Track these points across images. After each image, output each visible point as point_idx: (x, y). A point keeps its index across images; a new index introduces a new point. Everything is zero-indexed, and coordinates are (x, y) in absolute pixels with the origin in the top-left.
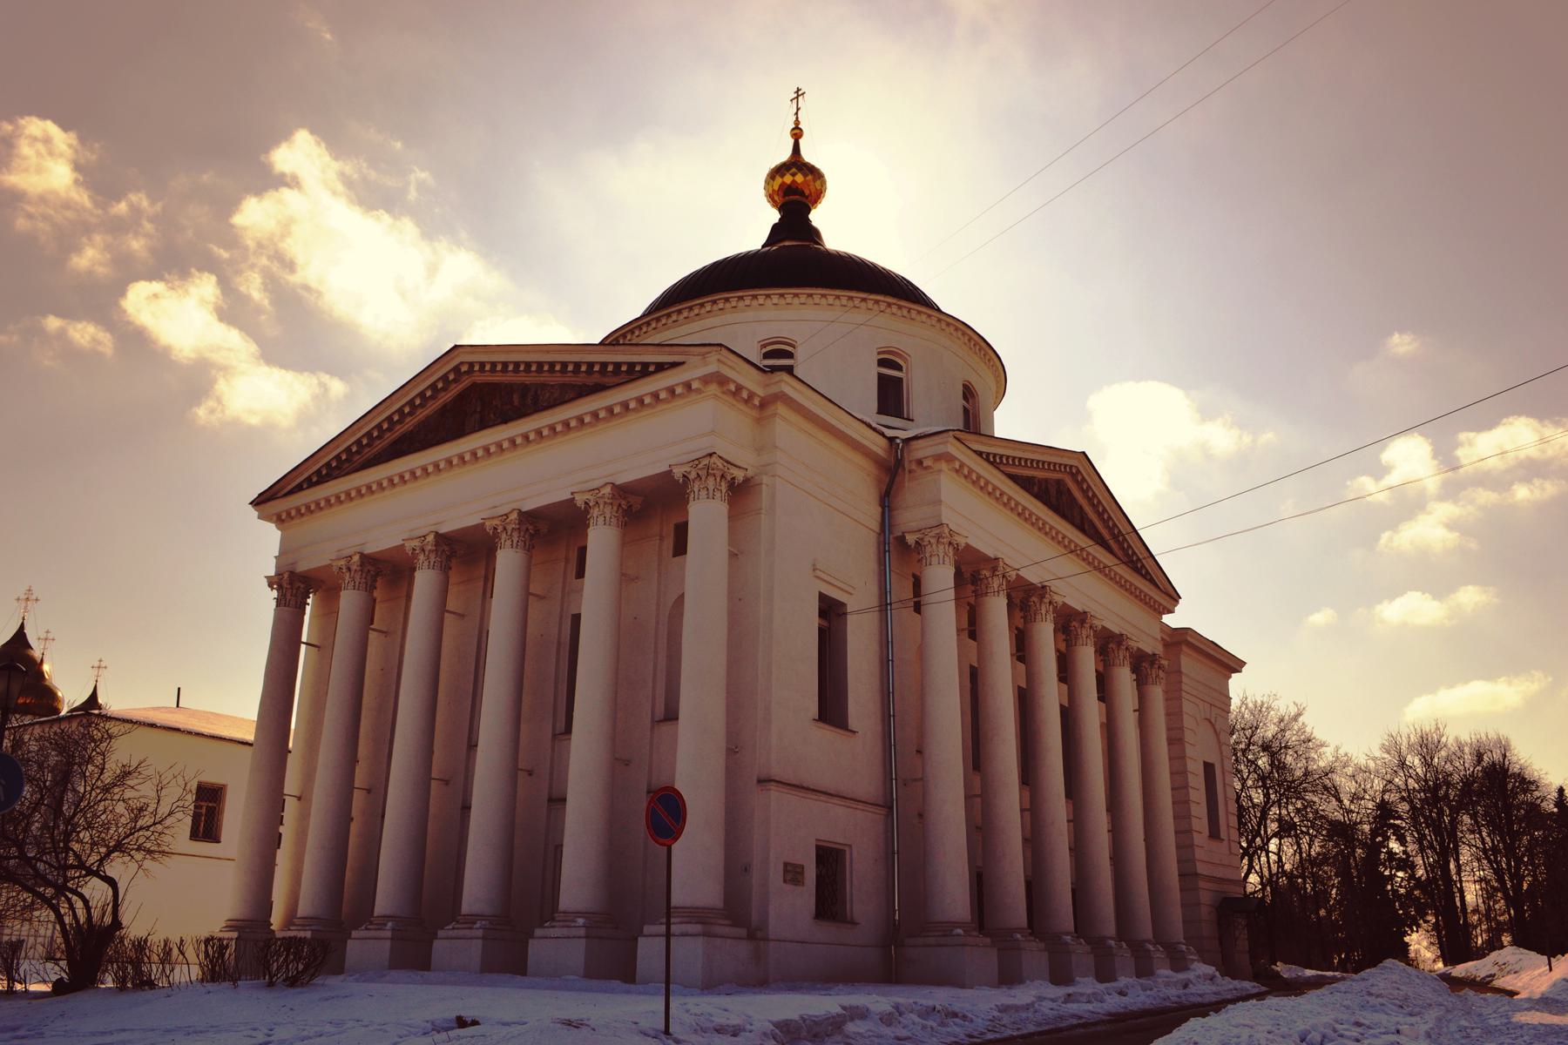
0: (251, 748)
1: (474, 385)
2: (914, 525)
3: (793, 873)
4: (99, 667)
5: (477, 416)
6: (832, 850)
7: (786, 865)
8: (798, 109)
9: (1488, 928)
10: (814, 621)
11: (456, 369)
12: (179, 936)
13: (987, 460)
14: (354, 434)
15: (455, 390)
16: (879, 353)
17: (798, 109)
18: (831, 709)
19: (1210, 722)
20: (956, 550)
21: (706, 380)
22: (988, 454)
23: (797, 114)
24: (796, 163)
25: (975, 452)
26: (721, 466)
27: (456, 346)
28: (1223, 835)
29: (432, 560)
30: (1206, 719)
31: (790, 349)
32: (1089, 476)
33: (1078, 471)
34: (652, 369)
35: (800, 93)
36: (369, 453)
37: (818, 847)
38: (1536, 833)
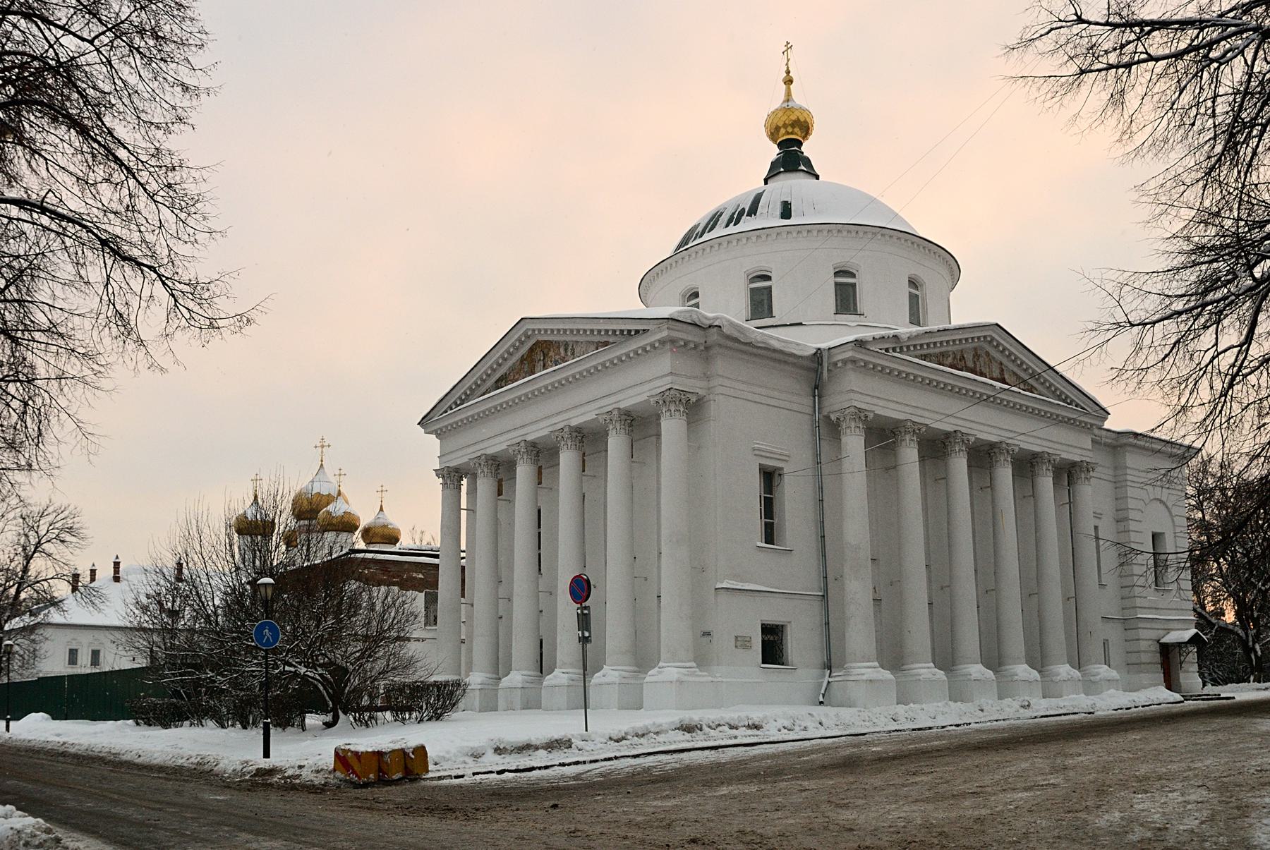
0: (4, 729)
1: (538, 342)
2: (836, 407)
3: (742, 642)
4: (340, 475)
5: (542, 363)
6: (777, 626)
8: (788, 60)
10: (755, 484)
11: (525, 334)
12: (465, 773)
16: (837, 274)
17: (788, 60)
19: (1161, 501)
20: (865, 421)
21: (662, 342)
23: (787, 64)
24: (788, 106)
27: (522, 319)
29: (525, 457)
30: (1155, 499)
34: (633, 333)
35: (789, 46)
37: (762, 625)
38: (267, 631)
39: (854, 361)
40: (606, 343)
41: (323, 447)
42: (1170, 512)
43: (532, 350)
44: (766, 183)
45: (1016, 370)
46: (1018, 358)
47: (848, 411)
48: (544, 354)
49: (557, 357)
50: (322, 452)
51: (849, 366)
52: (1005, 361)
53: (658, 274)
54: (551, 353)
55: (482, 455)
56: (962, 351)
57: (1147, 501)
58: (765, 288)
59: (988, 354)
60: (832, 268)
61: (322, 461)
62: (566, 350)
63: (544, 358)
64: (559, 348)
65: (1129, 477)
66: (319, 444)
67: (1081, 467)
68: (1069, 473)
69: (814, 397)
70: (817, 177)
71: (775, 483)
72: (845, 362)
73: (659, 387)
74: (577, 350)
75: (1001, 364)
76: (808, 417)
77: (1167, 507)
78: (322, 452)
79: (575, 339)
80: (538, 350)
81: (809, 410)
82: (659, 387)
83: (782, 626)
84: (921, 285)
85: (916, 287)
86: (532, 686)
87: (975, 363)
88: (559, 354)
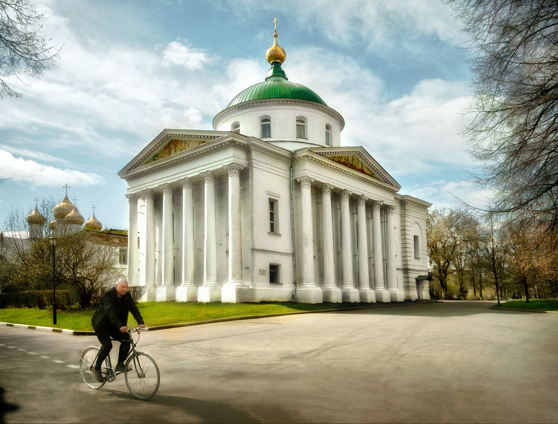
3: (262, 272)
5: (174, 149)
6: (275, 266)
7: (260, 270)
9: (481, 288)
13: (320, 154)
14: (142, 154)
15: (167, 142)
16: (297, 118)
18: (273, 229)
22: (320, 153)
25: (315, 153)
26: (236, 166)
27: (165, 129)
28: (421, 256)
31: (269, 119)
32: (364, 153)
33: (360, 152)
36: (147, 160)
39: (307, 156)
40: (204, 142)
41: (66, 187)
42: (421, 228)
43: (169, 144)
44: (266, 80)
45: (368, 166)
46: (337, 167)
47: (304, 178)
48: (175, 146)
49: (181, 147)
50: (66, 190)
51: (306, 158)
52: (363, 162)
53: (221, 116)
54: (178, 145)
55: (185, 178)
56: (348, 157)
57: (412, 223)
58: (266, 125)
59: (357, 158)
60: (296, 118)
61: (66, 193)
62: (185, 144)
63: (175, 147)
64: (182, 143)
65: (406, 213)
66: (65, 186)
67: (390, 208)
68: (385, 209)
69: (290, 171)
70: (287, 79)
71: (142, 306)
72: (304, 156)
73: (228, 162)
74: (190, 144)
75: (362, 163)
76: (287, 179)
77: (419, 226)
78: (66, 190)
79: (188, 139)
80: (172, 144)
81: (288, 177)
82: (228, 162)
83: (277, 266)
84: (330, 128)
85: (328, 129)
86: (171, 286)
87: (352, 162)
88: (182, 146)
